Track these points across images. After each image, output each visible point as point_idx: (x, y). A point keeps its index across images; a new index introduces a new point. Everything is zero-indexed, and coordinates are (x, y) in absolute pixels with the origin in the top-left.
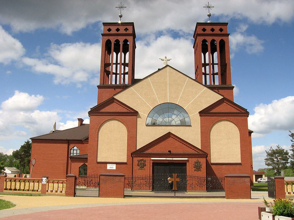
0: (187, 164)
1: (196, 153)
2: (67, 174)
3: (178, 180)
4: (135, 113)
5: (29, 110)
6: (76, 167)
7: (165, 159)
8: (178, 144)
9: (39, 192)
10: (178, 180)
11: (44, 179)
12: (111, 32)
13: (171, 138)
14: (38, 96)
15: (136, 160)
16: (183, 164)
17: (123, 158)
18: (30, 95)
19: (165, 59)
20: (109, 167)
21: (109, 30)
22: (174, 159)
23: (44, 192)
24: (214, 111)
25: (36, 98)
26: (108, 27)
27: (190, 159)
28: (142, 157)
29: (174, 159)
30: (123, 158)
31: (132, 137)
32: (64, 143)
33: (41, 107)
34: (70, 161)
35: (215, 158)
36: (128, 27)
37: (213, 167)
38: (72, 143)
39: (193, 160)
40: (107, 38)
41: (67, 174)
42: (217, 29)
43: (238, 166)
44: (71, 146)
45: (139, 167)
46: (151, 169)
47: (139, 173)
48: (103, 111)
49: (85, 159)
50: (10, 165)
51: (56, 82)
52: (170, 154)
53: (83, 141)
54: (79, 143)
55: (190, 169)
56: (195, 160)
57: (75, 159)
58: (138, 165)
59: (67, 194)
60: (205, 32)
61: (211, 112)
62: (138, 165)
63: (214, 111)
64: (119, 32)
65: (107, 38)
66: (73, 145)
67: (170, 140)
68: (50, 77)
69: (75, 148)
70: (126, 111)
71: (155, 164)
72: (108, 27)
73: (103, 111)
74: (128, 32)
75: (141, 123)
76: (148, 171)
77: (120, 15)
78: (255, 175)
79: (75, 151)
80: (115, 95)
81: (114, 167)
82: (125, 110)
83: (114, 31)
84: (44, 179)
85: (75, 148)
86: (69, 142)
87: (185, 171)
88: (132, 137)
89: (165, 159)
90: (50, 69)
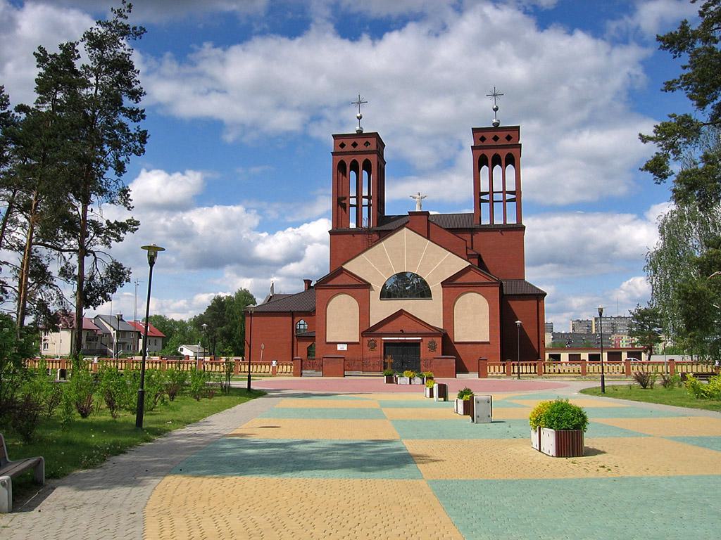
0: (421, 343)
1: (431, 332)
2: (293, 357)
3: (392, 361)
4: (367, 286)
5: (172, 207)
6: (303, 347)
7: (397, 338)
8: (411, 322)
9: (270, 373)
10: (392, 361)
11: (274, 362)
12: (345, 149)
13: (403, 316)
14: (190, 173)
15: (366, 340)
16: (417, 344)
17: (355, 338)
18: (170, 171)
19: (418, 196)
20: (340, 347)
21: (342, 145)
22: (407, 338)
23: (274, 373)
24: (458, 281)
25: (185, 178)
26: (340, 142)
27: (424, 339)
28: (372, 337)
29: (407, 338)
30: (355, 338)
31: (365, 313)
32: (288, 316)
33: (202, 199)
34: (295, 340)
35: (460, 335)
36: (369, 140)
37: (456, 346)
38: (298, 316)
39: (427, 340)
40: (339, 158)
41: (293, 357)
42: (502, 136)
43: (486, 345)
44: (296, 319)
45: (369, 348)
46: (383, 349)
47: (369, 353)
48: (330, 283)
49: (313, 338)
50: (189, 342)
51: (229, 138)
52: (402, 334)
53: (309, 314)
54: (306, 316)
55: (423, 347)
56: (430, 339)
57: (303, 338)
58: (368, 346)
59: (295, 375)
60: (485, 143)
61: (456, 282)
62: (368, 346)
63: (458, 281)
64: (357, 149)
65: (339, 158)
66: (299, 318)
67: (402, 317)
68: (213, 127)
69: (302, 322)
70: (358, 283)
71: (386, 344)
72: (340, 142)
73: (330, 283)
74: (369, 148)
75: (375, 295)
76: (379, 350)
77: (359, 115)
78: (608, 353)
79: (302, 324)
80: (343, 264)
81: (345, 347)
82: (355, 282)
83: (349, 148)
84: (274, 362)
85: (302, 322)
86: (293, 314)
87: (418, 353)
88: (365, 313)
89: (397, 338)
90: (211, 106)
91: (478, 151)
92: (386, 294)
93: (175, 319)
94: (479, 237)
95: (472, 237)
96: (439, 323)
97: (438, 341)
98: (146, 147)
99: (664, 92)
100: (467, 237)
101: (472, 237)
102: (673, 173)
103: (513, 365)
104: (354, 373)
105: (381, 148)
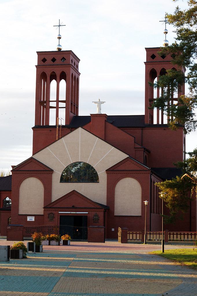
4: (51, 171)
20: (29, 219)
26: (65, 62)
29: (77, 213)
52: (74, 208)
58: (48, 217)
76: (56, 222)
81: (33, 219)
91: (70, 57)
92: (64, 179)
93: (175, 11)
94: (148, 132)
95: (159, 236)
96: (104, 202)
97: (101, 214)
98: (177, 35)
99: (165, 29)
100: (139, 131)
101: (159, 236)
102: (175, 41)
103: (170, 234)
104: (23, 265)
105: (76, 63)
